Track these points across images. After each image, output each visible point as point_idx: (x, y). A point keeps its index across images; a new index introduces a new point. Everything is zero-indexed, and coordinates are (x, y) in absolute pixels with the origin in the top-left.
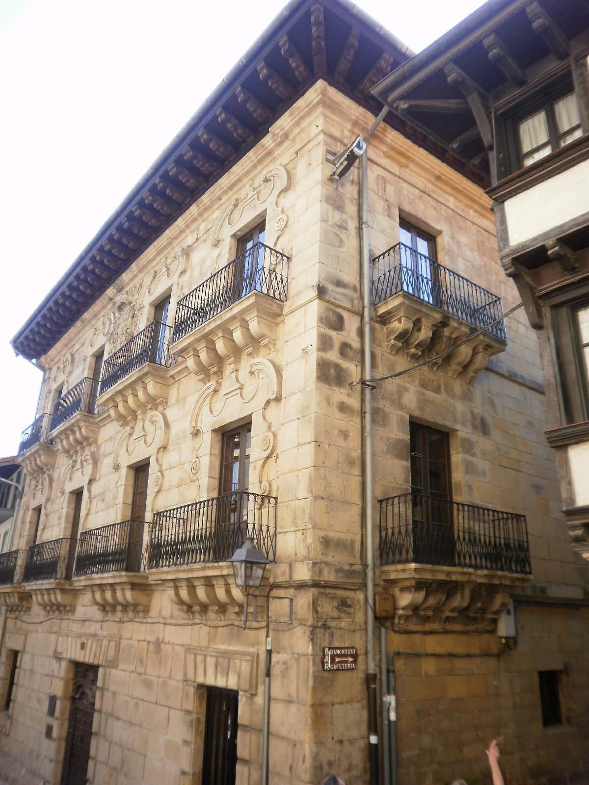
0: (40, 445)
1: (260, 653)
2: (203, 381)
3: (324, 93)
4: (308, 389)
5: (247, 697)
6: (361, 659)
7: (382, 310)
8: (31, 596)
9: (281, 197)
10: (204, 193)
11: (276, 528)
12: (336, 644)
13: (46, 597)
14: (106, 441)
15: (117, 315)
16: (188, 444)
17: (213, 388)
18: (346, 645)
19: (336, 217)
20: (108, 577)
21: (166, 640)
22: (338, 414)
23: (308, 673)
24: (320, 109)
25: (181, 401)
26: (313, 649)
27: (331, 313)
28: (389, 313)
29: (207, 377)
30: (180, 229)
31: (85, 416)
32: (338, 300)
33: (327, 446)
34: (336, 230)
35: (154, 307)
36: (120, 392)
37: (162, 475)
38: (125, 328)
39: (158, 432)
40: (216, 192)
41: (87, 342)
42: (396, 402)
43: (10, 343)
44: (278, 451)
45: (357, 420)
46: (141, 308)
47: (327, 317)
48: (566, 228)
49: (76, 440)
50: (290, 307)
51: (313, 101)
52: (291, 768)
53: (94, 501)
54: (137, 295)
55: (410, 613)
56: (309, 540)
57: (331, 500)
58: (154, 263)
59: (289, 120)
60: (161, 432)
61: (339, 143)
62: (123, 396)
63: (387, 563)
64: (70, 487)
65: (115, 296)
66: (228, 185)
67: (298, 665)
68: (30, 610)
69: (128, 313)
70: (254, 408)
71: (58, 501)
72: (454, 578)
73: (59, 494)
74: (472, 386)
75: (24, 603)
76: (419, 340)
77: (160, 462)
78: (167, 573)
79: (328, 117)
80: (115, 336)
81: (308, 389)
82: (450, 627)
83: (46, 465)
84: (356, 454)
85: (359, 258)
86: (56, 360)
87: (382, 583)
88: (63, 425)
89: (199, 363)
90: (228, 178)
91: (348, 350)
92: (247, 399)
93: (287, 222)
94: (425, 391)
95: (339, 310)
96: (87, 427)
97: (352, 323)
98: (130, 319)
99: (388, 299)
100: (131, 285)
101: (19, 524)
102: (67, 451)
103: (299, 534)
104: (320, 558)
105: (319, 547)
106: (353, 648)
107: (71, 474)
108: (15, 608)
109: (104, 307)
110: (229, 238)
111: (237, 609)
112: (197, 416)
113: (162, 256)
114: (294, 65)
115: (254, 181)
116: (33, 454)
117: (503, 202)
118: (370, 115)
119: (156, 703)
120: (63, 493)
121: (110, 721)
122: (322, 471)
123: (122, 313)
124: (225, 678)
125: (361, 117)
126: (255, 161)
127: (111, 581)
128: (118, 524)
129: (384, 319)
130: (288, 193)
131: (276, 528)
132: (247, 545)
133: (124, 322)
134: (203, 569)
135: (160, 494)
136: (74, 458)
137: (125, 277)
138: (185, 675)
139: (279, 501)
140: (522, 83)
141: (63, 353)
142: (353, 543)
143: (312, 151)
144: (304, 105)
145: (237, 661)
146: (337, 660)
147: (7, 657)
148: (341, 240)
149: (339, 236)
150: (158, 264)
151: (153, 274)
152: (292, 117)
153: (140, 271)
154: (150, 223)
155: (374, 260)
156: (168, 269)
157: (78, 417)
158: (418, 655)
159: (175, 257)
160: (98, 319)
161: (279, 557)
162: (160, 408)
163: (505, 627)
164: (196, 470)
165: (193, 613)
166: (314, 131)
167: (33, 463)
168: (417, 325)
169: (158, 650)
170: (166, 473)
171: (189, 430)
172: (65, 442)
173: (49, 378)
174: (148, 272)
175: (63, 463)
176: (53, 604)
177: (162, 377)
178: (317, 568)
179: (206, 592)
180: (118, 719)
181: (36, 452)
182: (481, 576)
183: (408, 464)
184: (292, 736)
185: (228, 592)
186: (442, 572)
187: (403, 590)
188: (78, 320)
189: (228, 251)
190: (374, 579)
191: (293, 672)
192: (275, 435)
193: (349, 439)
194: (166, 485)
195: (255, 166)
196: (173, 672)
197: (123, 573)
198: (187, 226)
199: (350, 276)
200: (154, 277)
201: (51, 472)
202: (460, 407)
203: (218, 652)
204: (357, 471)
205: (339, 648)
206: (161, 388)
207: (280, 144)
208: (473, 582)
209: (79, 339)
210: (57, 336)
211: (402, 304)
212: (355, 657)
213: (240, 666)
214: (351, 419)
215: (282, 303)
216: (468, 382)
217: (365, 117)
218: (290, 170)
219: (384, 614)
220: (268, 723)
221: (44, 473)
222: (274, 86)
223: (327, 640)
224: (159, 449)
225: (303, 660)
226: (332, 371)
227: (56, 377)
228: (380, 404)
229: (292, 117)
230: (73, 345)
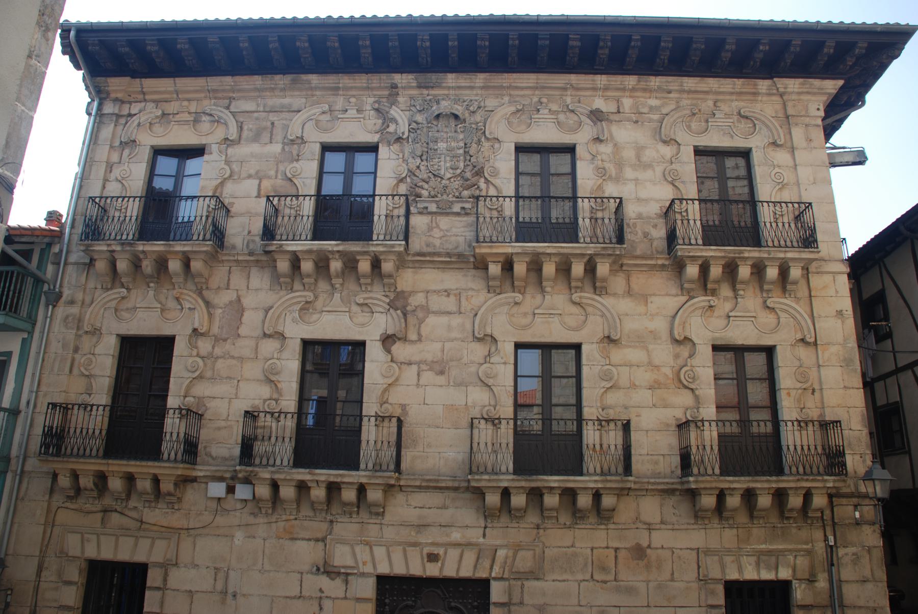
40: (672, 84)
90: (696, 83)
119: (648, 606)
153: (482, 88)
184: (871, 604)
195: (732, 93)
203: (756, 552)
220: (177, 555)
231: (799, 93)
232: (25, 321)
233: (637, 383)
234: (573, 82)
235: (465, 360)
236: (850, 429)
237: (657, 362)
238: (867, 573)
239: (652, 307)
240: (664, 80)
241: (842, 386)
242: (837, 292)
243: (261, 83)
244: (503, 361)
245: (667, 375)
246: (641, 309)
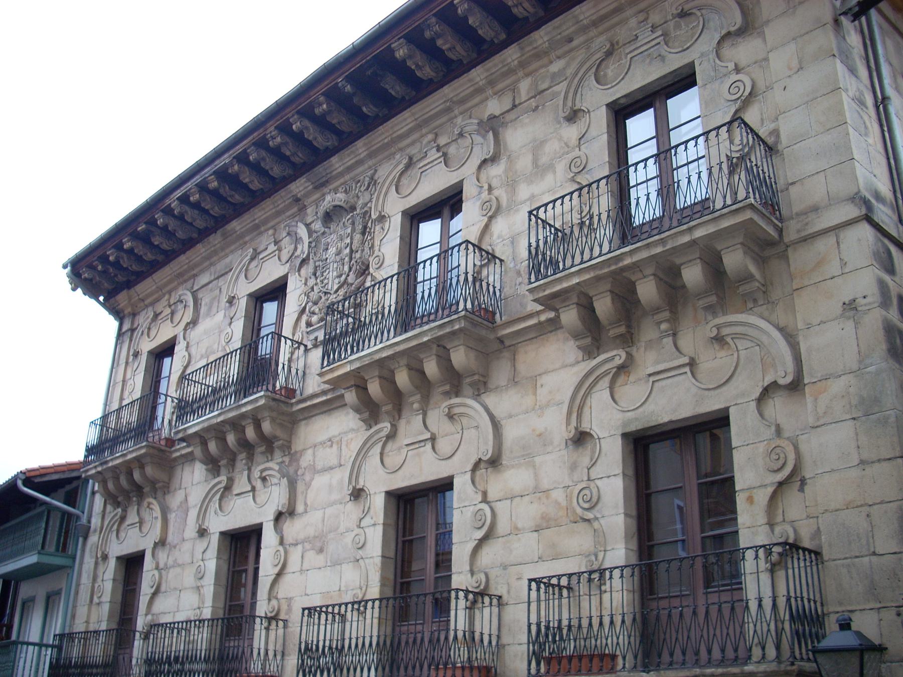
2: (589, 352)
9: (727, 44)
17: (223, 485)
30: (476, 86)
35: (409, 217)
46: (382, 218)
66: (594, 17)
71: (187, 546)
96: (273, 420)
150: (413, 143)
153: (370, 156)
157: (262, 402)
198: (491, 83)
232: (55, 556)
233: (520, 525)
234: (451, 95)
235: (342, 529)
236: (874, 554)
237: (545, 484)
239: (542, 393)
241: (856, 462)
242: (844, 264)
243: (204, 250)
244: (372, 522)
245: (559, 504)
246: (529, 401)
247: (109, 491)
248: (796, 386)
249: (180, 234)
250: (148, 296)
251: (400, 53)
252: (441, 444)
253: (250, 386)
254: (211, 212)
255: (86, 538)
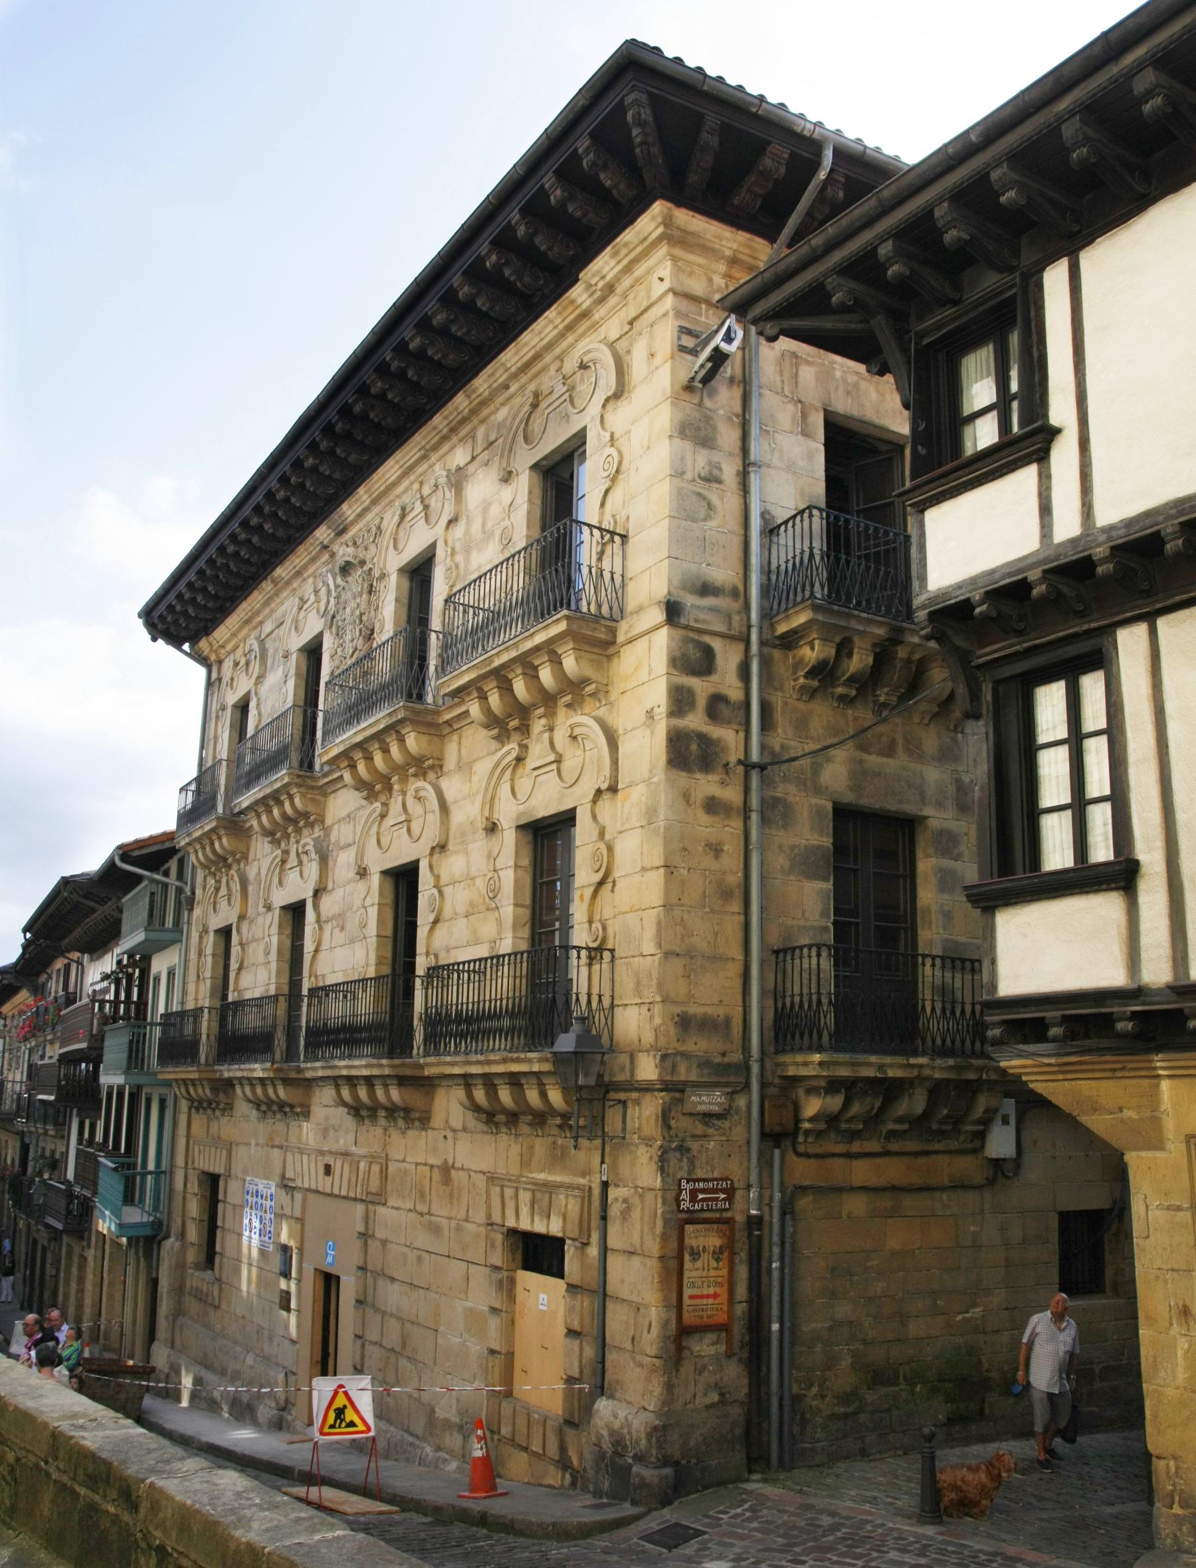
0: (218, 818)
1: (593, 1185)
3: (667, 222)
4: (655, 780)
5: (576, 1248)
6: (739, 1195)
7: (782, 628)
8: (233, 1086)
9: (610, 407)
10: (476, 375)
11: (613, 997)
12: (700, 1174)
13: (259, 1090)
14: (339, 821)
15: (339, 581)
16: (479, 845)
17: (514, 755)
18: (716, 1175)
19: (700, 461)
20: (360, 1065)
21: (458, 1165)
22: (704, 818)
23: (655, 1214)
24: (663, 250)
25: (465, 767)
26: (663, 1180)
27: (690, 646)
28: (794, 632)
29: (502, 737)
31: (298, 776)
32: (704, 621)
33: (685, 872)
34: (701, 487)
35: (407, 575)
36: (360, 746)
37: (441, 893)
38: (358, 613)
39: (430, 817)
40: (497, 375)
41: (288, 621)
42: (809, 784)
43: (140, 616)
44: (617, 873)
45: (737, 824)
46: (383, 576)
47: (683, 655)
48: (997, 576)
49: (284, 815)
50: (626, 633)
51: (650, 234)
52: (633, 1339)
53: (328, 928)
54: (372, 548)
55: (823, 1126)
56: (658, 1021)
57: (691, 958)
58: (399, 489)
59: (613, 263)
60: (434, 818)
61: (704, 306)
62: (365, 750)
63: (784, 1051)
64: (281, 898)
65: (332, 541)
66: (519, 365)
67: (642, 1202)
68: (231, 1109)
69: (360, 581)
70: (579, 798)
71: (260, 920)
72: (891, 1073)
73: (262, 910)
74: (962, 732)
75: (222, 1097)
76: (848, 674)
77: (436, 872)
78: (453, 1064)
79: (681, 259)
80: (340, 623)
81: (655, 780)
82: (894, 1146)
83: (233, 854)
84: (735, 879)
85: (742, 532)
86: (229, 647)
87: (777, 1081)
88: (260, 790)
89: (487, 711)
91: (722, 706)
92: (569, 777)
93: (620, 463)
94: (866, 757)
95: (707, 639)
96: (303, 796)
97: (728, 658)
98: (365, 596)
99: (791, 612)
100: (360, 525)
101: (193, 955)
102: (269, 833)
103: (644, 1008)
104: (674, 1046)
105: (672, 1030)
106: (726, 1179)
107: (280, 874)
108: (205, 1105)
109: (313, 560)
110: (527, 472)
111: (558, 1121)
112: (493, 798)
113: (412, 478)
114: (608, 183)
115: (562, 361)
116: (207, 835)
117: (922, 512)
118: (760, 244)
120: (269, 908)
121: (380, 1283)
122: (677, 913)
123: (350, 579)
124: (545, 1222)
125: (741, 249)
126: (561, 327)
127: (365, 1072)
128: (371, 979)
129: (789, 641)
130: (619, 403)
131: (613, 997)
132: (576, 1027)
133: (354, 598)
134: (505, 1061)
135: (439, 925)
136: (283, 845)
137: (348, 509)
138: (489, 1216)
139: (617, 954)
140: (955, 303)
141: (240, 636)
142: (728, 1021)
143: (656, 327)
144: (636, 241)
145: (562, 1197)
146: (701, 1196)
147: (200, 1183)
148: (710, 506)
149: (705, 498)
150: (406, 491)
151: (399, 512)
152: (618, 258)
153: (374, 502)
154: (383, 423)
155: (771, 531)
156: (426, 507)
157: (286, 780)
158: (839, 1190)
159: (436, 486)
160: (305, 580)
161: (618, 1043)
162: (431, 775)
163: (1001, 1143)
164: (494, 893)
165: (497, 1125)
166: (659, 289)
167: (208, 849)
168: (844, 648)
169: (447, 1180)
170: (447, 891)
171: (481, 824)
172: (264, 818)
173: (220, 679)
174: (391, 503)
175: (262, 853)
176: (272, 1101)
177: (430, 725)
178: (668, 1063)
179: (512, 1094)
180: (393, 1279)
181: (213, 830)
182: (941, 1069)
183: (828, 886)
184: (634, 1298)
185: (543, 1095)
186: (870, 1065)
187: (810, 1091)
188: (265, 578)
189: (526, 498)
190: (762, 1074)
191: (636, 1214)
192: (610, 849)
193: (724, 855)
194: (447, 912)
195: (562, 336)
196: (471, 1211)
197: (384, 1062)
199: (724, 573)
200: (403, 516)
201: (242, 865)
202: (933, 775)
204: (736, 906)
205: (704, 1180)
206: (430, 742)
207: (602, 300)
208: (928, 1078)
209: (272, 611)
210: (228, 605)
211: (810, 622)
212: (730, 1193)
213: (566, 1206)
214: (726, 823)
215: (614, 624)
216: (952, 727)
217: (751, 248)
218: (621, 352)
219: (777, 1129)
221: (229, 867)
222: (578, 214)
223: (686, 1168)
224: (433, 848)
225: (649, 1196)
226: (694, 747)
227: (232, 679)
228: (779, 792)
229: (618, 258)
230: (261, 623)
231: (628, 269)
238: (636, 1239)
240: (485, 376)
247: (495, 715)
248: (613, 789)
249: (254, 559)
250: (227, 642)
251: (556, 195)
252: (568, 765)
253: (495, 631)
254: (491, 314)
255: (191, 910)
